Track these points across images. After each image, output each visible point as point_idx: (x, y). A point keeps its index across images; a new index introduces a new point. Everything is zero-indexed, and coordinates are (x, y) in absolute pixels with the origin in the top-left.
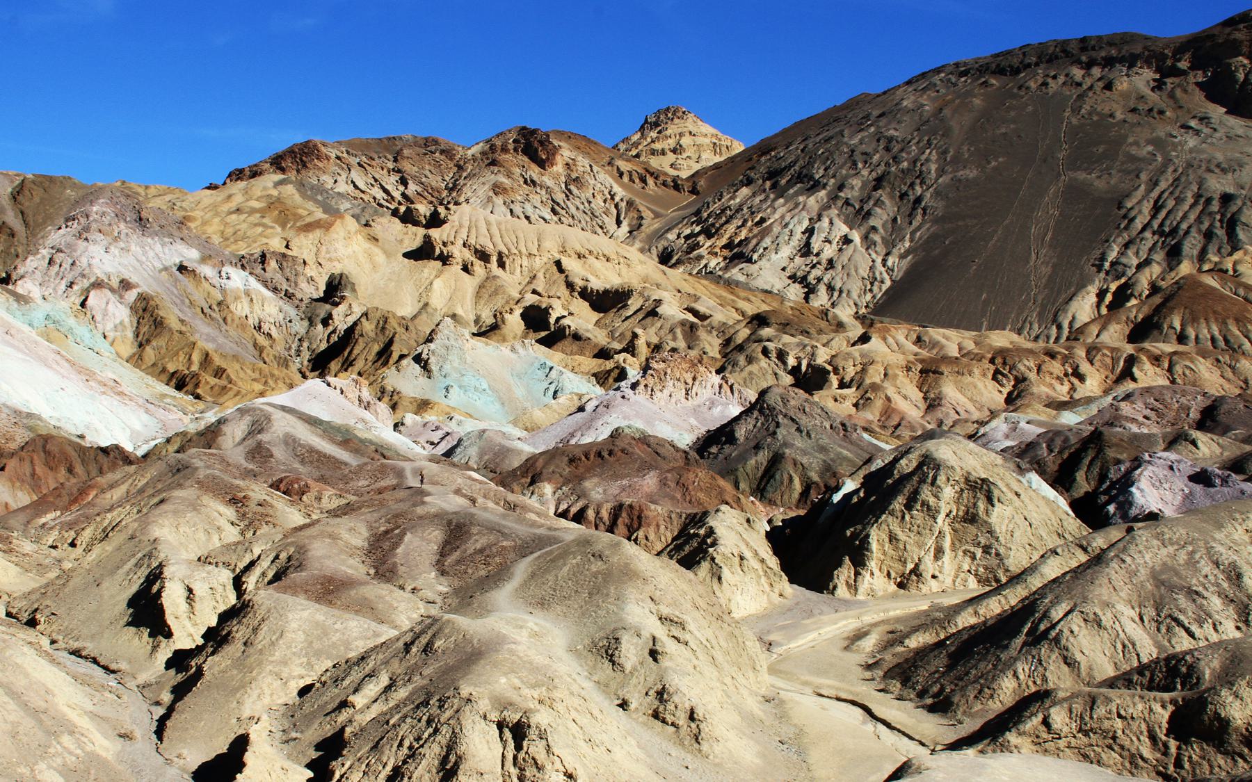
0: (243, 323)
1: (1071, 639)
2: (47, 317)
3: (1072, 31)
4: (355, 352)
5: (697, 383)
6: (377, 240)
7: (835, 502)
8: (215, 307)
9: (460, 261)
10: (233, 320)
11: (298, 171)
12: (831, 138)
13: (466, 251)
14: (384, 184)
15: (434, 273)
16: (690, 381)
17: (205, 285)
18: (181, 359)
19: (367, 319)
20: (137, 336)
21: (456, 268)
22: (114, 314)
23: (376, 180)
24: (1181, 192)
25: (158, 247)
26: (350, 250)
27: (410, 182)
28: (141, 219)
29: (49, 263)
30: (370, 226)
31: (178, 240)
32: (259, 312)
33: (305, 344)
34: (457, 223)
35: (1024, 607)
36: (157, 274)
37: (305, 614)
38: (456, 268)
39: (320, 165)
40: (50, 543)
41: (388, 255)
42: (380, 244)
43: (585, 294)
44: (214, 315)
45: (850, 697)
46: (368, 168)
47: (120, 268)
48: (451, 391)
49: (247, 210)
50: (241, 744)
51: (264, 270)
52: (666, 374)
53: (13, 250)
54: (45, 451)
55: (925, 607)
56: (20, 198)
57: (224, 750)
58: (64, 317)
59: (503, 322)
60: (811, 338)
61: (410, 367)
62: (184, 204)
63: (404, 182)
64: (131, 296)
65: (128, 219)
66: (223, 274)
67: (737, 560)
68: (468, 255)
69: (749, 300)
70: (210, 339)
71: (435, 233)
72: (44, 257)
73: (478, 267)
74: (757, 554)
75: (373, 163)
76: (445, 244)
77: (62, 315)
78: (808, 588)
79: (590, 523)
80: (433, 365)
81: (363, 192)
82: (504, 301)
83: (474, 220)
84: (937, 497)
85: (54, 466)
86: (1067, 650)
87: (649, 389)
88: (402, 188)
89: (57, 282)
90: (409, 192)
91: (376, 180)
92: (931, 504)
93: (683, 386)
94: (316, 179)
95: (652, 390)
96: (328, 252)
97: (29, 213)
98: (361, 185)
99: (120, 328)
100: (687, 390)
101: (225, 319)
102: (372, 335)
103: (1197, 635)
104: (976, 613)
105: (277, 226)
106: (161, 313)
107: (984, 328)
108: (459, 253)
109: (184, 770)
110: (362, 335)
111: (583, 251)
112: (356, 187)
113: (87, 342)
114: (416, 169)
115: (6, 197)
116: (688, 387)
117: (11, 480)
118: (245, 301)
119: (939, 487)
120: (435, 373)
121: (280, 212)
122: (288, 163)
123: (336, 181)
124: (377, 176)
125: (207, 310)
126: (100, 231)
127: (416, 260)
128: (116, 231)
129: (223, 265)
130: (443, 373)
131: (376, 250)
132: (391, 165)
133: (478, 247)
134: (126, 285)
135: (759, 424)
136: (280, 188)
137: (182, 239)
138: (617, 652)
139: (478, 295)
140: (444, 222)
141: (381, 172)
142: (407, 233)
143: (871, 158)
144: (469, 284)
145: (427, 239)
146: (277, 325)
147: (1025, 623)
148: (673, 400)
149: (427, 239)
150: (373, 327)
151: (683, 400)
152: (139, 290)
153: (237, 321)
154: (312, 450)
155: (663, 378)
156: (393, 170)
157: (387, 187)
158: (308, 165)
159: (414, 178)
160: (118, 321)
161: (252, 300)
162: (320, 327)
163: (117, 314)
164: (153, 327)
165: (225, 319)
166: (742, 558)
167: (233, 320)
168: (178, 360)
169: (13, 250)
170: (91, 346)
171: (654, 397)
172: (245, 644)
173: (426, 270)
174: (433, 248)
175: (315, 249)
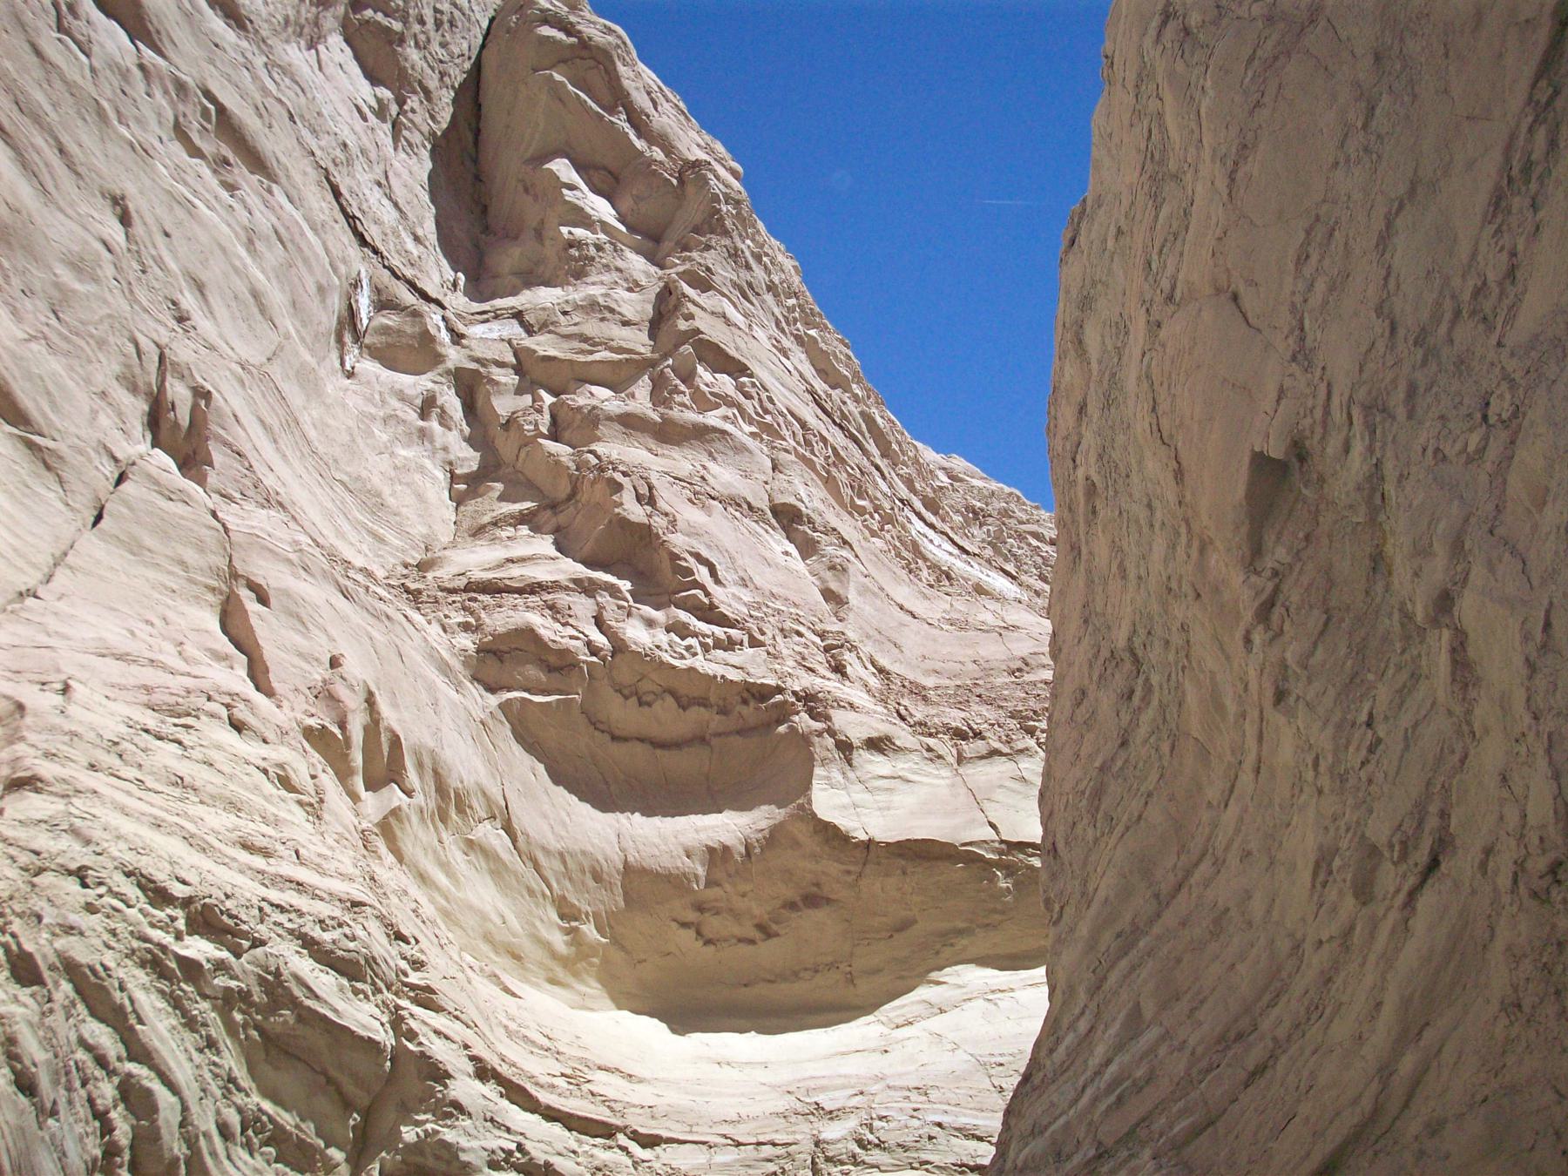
3: (509, 997)
7: (465, 486)
12: (28, 487)
20: (963, 578)
24: (351, 688)
35: (546, 644)
37: (460, 895)
40: (980, 743)
43: (45, 870)
45: (492, 31)
50: (724, 586)
55: (735, 679)
57: (753, 1033)
60: (145, 130)
69: (82, 323)
78: (704, 813)
103: (186, 742)
104: (650, 516)
105: (425, 155)
109: (4, 1032)
111: (116, 740)
127: (580, 800)
138: (368, 988)
143: (429, 457)
147: (999, 480)
154: (254, 260)
162: (1253, 846)
172: (526, 190)
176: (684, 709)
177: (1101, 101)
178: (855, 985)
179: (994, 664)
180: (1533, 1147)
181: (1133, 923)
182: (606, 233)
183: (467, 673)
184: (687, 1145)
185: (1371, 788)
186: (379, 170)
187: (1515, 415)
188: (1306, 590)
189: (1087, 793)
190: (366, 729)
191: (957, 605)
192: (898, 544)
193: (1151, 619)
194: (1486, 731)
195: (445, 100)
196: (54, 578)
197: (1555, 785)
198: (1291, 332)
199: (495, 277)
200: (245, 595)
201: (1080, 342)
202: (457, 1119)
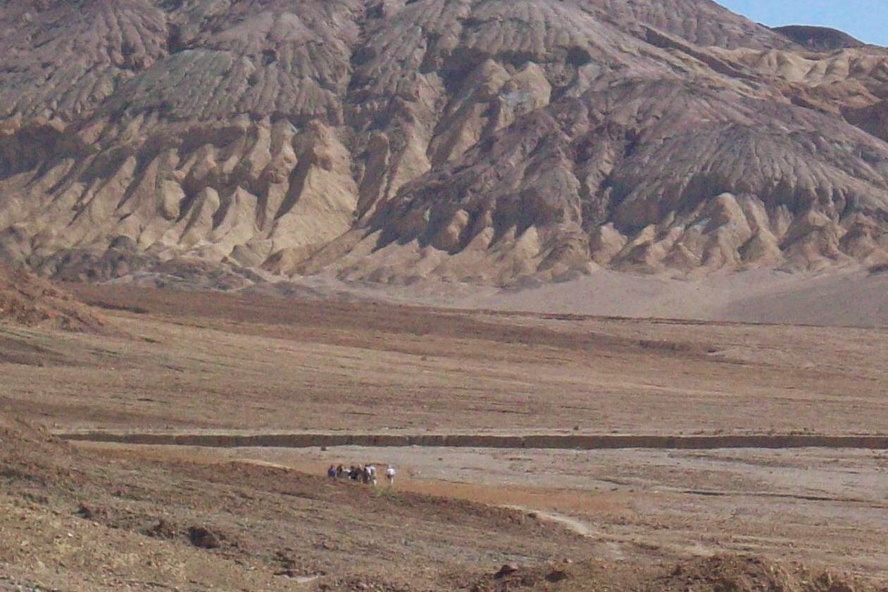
4: (417, 305)
190: (186, 212)
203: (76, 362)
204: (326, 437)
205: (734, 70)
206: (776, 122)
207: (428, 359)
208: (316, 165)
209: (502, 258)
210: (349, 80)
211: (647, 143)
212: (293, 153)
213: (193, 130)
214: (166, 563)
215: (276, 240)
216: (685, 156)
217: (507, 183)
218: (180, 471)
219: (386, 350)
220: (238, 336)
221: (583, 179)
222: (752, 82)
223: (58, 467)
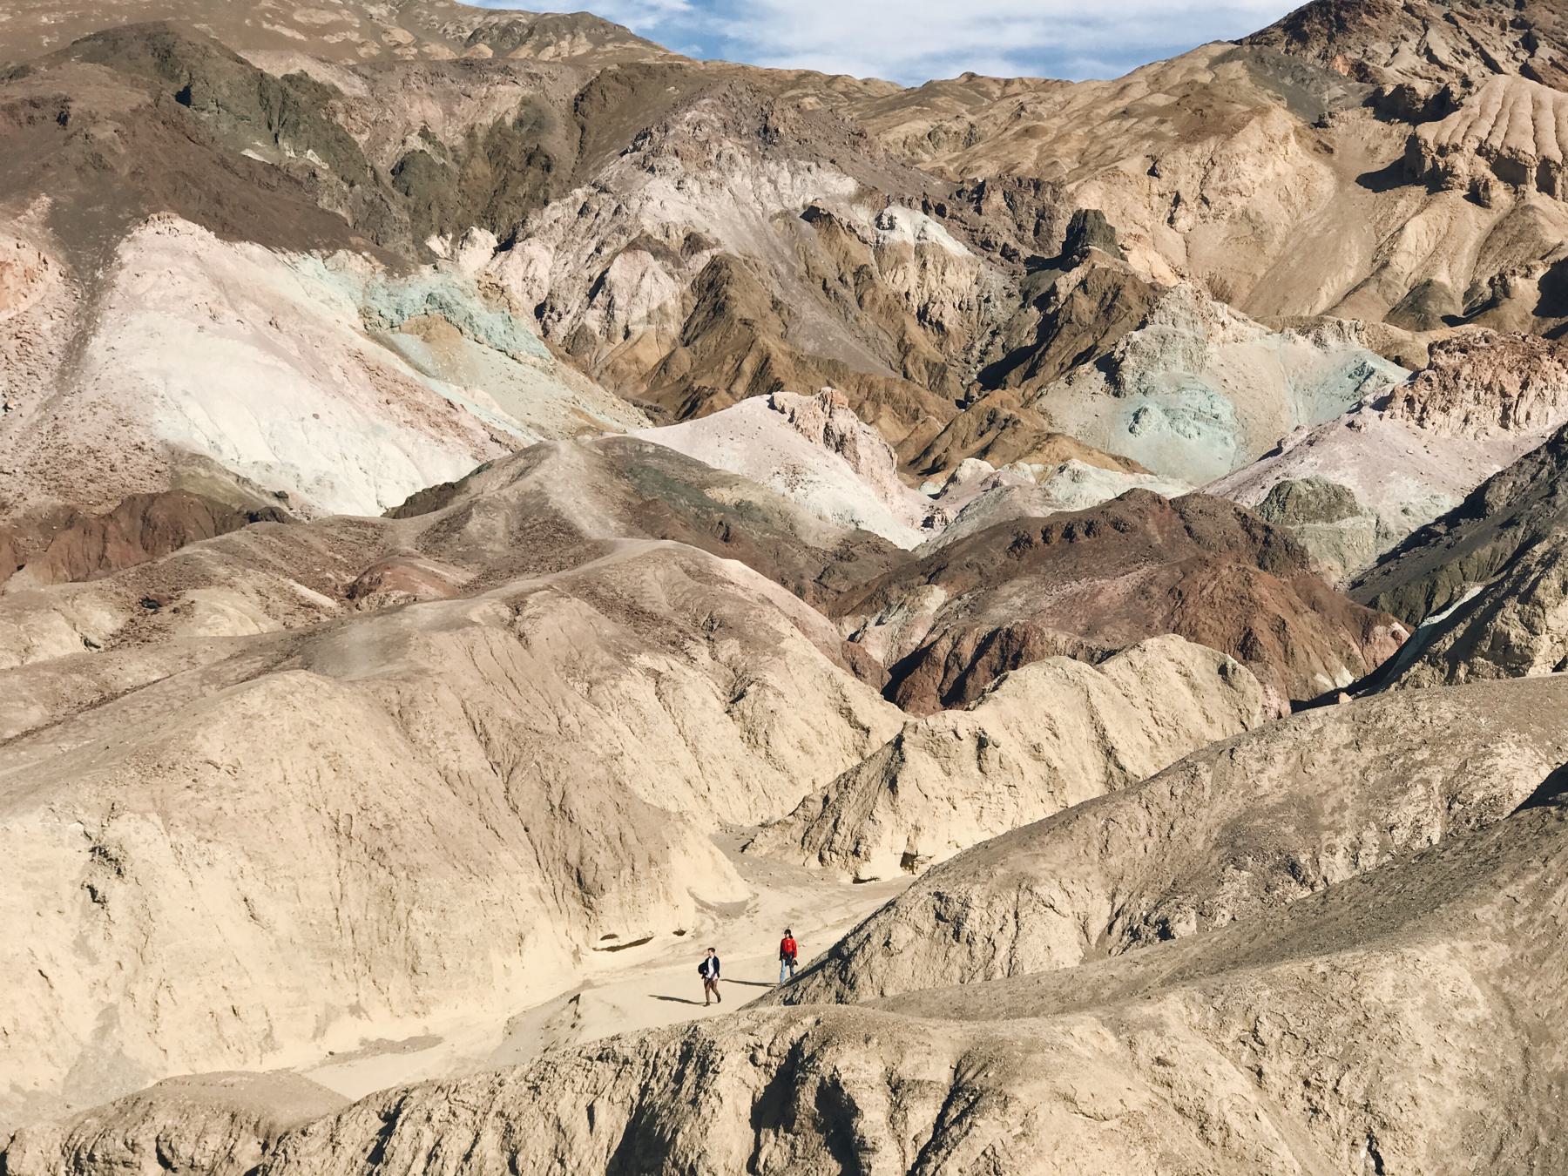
0: (893, 307)
1: (879, 960)
2: (430, 298)
4: (1051, 351)
5: (1531, 393)
6: (1330, 151)
8: (850, 279)
9: (1467, 180)
10: (874, 300)
11: (1331, 39)
13: (1481, 160)
14: (1489, 50)
15: (1416, 206)
16: (1514, 391)
17: (844, 238)
18: (726, 368)
19: (1086, 292)
21: (1457, 195)
22: (649, 294)
23: (1474, 44)
25: (785, 177)
26: (1269, 172)
27: (1542, 43)
28: (766, 130)
29: (581, 213)
30: (1325, 126)
31: (826, 164)
32: (934, 284)
33: (999, 340)
34: (1477, 110)
36: (765, 221)
38: (1457, 195)
39: (1372, 23)
41: (1339, 172)
42: (1335, 158)
44: (843, 291)
46: (1463, 22)
47: (697, 216)
48: (1143, 419)
49: (1142, 110)
51: (978, 210)
52: (1457, 376)
53: (541, 194)
54: (144, 519)
56: (585, 105)
58: (459, 296)
59: (1507, 294)
61: (1092, 377)
62: (1040, 108)
63: (1530, 44)
64: (701, 261)
65: (744, 131)
66: (885, 221)
67: (969, 745)
68: (1483, 168)
70: (819, 333)
71: (1429, 132)
72: (575, 202)
73: (1501, 194)
74: (1103, 737)
75: (1476, 13)
76: (1442, 151)
77: (456, 293)
79: (937, 664)
80: (1128, 377)
81: (1444, 67)
82: (1528, 254)
83: (1511, 100)
84: (1532, 629)
85: (151, 543)
86: (852, 987)
87: (1418, 407)
88: (1523, 55)
89: (585, 242)
90: (1536, 63)
91: (1474, 44)
92: (1513, 640)
93: (1497, 400)
94: (1360, 49)
95: (1424, 409)
96: (1223, 178)
97: (592, 129)
98: (1443, 54)
99: (657, 316)
100: (1506, 409)
101: (860, 300)
102: (1088, 319)
106: (732, 292)
107: (1280, 231)
108: (1465, 165)
110: (1069, 321)
112: (1432, 59)
113: (496, 339)
114: (1557, 18)
115: (563, 105)
116: (1507, 401)
117: (53, 567)
118: (913, 268)
119: (1540, 604)
120: (1128, 386)
121: (1195, 112)
122: (1313, 25)
123: (1396, 51)
124: (1478, 37)
125: (834, 284)
126: (677, 154)
128: (715, 152)
129: (889, 203)
130: (1143, 387)
131: (1323, 170)
132: (1509, 15)
133: (1505, 152)
134: (694, 243)
135: (1545, 472)
136: (1219, 69)
137: (833, 161)
139: (1486, 246)
140: (1456, 107)
141: (1488, 29)
142: (1390, 135)
144: (1476, 220)
145: (1413, 143)
146: (964, 306)
148: (1471, 430)
149: (1413, 143)
150: (1096, 305)
151: (1495, 428)
152: (715, 252)
153: (881, 299)
155: (1450, 383)
156: (1513, 23)
157: (1493, 55)
158: (1350, 25)
159: (1550, 35)
160: (655, 306)
161: (924, 265)
163: (656, 294)
164: (711, 314)
165: (860, 300)
166: (982, 743)
167: (874, 300)
168: (720, 371)
169: (541, 194)
170: (504, 346)
171: (1427, 423)
173: (1402, 203)
174: (1420, 159)
175: (1200, 173)
176: (315, 749)
177: (1067, 510)
178: (1158, 176)
179: (1540, 112)
180: (53, 1031)
181: (1532, 208)
182: (389, 608)
183: (638, 414)
184: (627, 942)
185: (420, 994)
186: (388, 869)
187: (455, 425)
188: (795, 979)
189: (379, 421)
191: (22, 421)
192: (1329, 916)
193: (555, 1049)
194: (206, 48)
195: (432, 111)
196: (656, 698)
197: (539, 326)
198: (933, 107)
199: (550, 133)
200: (1027, 364)
201: (1236, 964)
202: (408, 670)
203: (1024, 845)
204: (754, 564)
205: (1451, 610)
206: (1538, 876)
207: (975, 287)
208: (207, 580)
209: (256, 1126)
210: (146, 234)
211: (1324, 213)
212: (969, 657)
213: (980, 375)
214: (808, 814)
215: (818, 272)
216: (1169, 719)
217: (411, 702)
218: (1112, 789)
219: (1262, 33)
220: (546, 462)
221: (60, 56)
222: (1460, 631)
223: (216, 721)
